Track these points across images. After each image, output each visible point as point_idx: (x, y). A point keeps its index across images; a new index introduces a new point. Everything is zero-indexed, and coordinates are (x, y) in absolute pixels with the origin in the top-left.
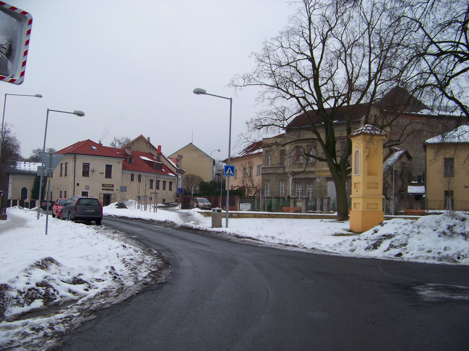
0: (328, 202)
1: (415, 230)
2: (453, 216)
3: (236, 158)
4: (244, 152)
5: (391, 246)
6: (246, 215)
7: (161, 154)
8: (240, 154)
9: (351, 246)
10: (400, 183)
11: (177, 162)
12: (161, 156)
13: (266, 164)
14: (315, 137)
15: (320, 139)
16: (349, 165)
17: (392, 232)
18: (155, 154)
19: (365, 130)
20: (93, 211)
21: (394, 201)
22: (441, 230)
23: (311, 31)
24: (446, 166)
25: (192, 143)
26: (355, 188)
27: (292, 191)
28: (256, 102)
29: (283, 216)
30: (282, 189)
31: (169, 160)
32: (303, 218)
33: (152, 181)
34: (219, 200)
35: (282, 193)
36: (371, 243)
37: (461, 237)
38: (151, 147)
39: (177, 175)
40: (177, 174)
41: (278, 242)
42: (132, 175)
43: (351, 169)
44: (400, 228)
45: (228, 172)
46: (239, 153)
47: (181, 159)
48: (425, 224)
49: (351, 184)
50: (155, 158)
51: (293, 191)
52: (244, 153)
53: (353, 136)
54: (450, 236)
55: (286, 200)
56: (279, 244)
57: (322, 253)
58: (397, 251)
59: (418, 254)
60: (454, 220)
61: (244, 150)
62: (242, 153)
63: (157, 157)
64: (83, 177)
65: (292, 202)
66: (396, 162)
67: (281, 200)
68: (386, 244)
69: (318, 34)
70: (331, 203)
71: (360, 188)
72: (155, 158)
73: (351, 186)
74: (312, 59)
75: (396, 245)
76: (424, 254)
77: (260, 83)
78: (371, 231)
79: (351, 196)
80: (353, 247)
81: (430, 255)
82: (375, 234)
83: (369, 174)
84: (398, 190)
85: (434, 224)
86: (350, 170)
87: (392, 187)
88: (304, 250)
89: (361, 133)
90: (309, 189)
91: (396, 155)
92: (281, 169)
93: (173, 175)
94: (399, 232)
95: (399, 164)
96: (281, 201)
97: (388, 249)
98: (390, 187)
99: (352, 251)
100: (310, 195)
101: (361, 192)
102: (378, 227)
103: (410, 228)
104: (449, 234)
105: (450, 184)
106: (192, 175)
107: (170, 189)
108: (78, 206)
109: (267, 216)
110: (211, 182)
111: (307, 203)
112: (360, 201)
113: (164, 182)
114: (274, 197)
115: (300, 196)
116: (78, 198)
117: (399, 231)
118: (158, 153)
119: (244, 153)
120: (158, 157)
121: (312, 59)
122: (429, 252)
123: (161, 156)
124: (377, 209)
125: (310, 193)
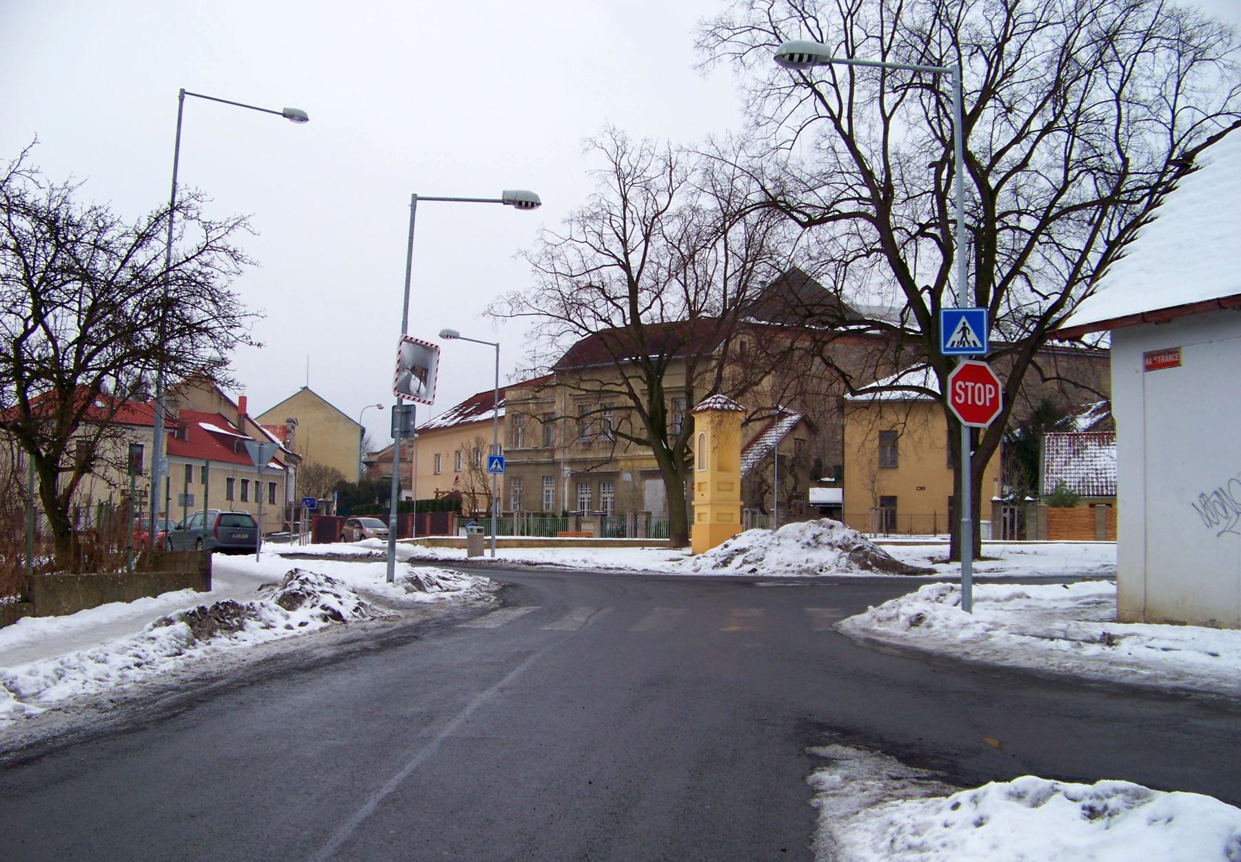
0: (647, 522)
1: (774, 542)
2: (820, 524)
3: (439, 428)
4: (456, 414)
5: (745, 562)
6: (505, 543)
7: (246, 416)
8: (448, 419)
9: (694, 565)
10: (790, 481)
11: (285, 437)
12: (247, 422)
13: (512, 443)
14: (631, 403)
15: (639, 407)
16: (690, 451)
17: (746, 546)
18: (232, 416)
19: (715, 403)
20: (246, 536)
21: (777, 517)
22: (805, 540)
23: (627, 220)
24: (882, 446)
25: (306, 388)
26: (699, 490)
27: (570, 501)
28: (526, 340)
29: (573, 543)
30: (548, 497)
31: (265, 430)
32: (609, 546)
33: (230, 481)
34: (410, 522)
35: (549, 505)
36: (720, 560)
37: (827, 547)
38: (221, 399)
39: (286, 467)
40: (286, 464)
41: (595, 566)
42: (189, 467)
43: (693, 458)
44: (757, 540)
45: (494, 466)
46: (443, 416)
47: (293, 427)
48: (787, 535)
49: (693, 484)
50: (231, 425)
51: (573, 501)
52: (456, 417)
53: (696, 412)
54: (815, 547)
55: (560, 518)
56: (597, 567)
57: (658, 574)
58: (750, 567)
59: (777, 568)
60: (821, 528)
61: (456, 411)
62: (452, 417)
63: (236, 424)
64: (947, 499)
65: (571, 522)
66: (784, 438)
67: (549, 518)
68: (738, 560)
69: (637, 221)
70: (654, 522)
71: (706, 490)
72: (231, 425)
73: (693, 488)
74: (626, 267)
75: (750, 560)
76: (782, 568)
77: (537, 312)
78: (721, 546)
79: (693, 503)
80: (698, 566)
81: (789, 569)
82: (725, 549)
83: (720, 469)
84: (786, 494)
85: (797, 534)
86: (692, 460)
87: (773, 488)
88: (635, 573)
89: (707, 409)
90: (582, 496)
91: (786, 423)
92: (546, 454)
93: (278, 467)
94: (755, 545)
95: (790, 444)
96: (548, 522)
97: (741, 566)
98: (771, 490)
99: (697, 571)
100: (609, 509)
101: (708, 496)
102: (730, 541)
103: (769, 539)
104: (813, 544)
105: (876, 483)
106: (318, 467)
107: (272, 501)
108: (220, 528)
109: (542, 543)
110: (361, 483)
111: (602, 524)
112: (707, 510)
113: (245, 482)
114: (534, 514)
115: (586, 510)
116: (217, 514)
117: (756, 544)
118: (240, 415)
119: (456, 417)
120: (239, 423)
121: (626, 267)
122: (788, 565)
123: (247, 422)
124: (732, 521)
125: (609, 505)
